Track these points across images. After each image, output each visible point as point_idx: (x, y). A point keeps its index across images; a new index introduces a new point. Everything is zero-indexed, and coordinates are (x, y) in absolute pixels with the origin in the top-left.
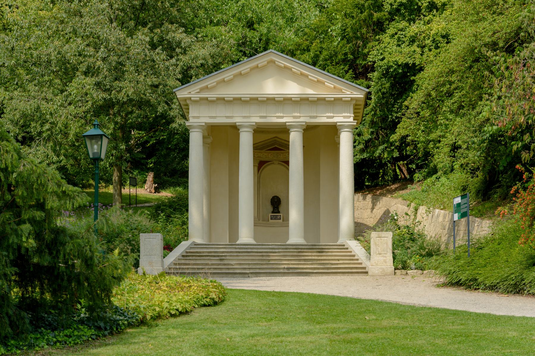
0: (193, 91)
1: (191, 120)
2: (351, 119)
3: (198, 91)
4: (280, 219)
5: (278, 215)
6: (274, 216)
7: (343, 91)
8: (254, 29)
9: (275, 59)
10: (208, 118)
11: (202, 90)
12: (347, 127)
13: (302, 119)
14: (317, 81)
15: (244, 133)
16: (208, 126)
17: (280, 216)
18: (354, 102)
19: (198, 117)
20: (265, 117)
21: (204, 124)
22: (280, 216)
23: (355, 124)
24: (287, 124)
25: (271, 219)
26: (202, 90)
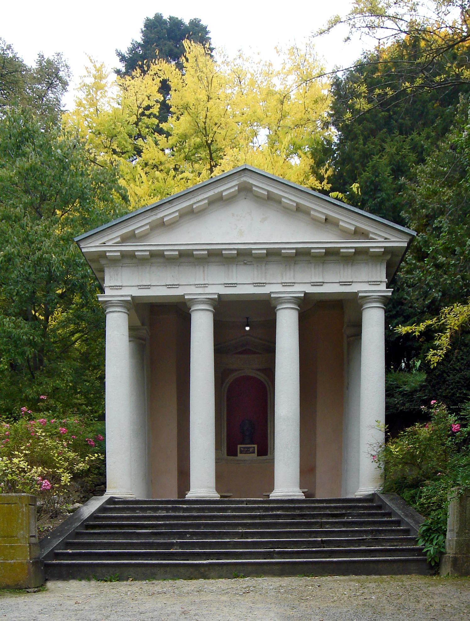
0: (108, 241)
1: (108, 292)
2: (383, 287)
3: (119, 239)
4: (254, 452)
5: (251, 447)
6: (244, 448)
7: (371, 235)
8: (134, 124)
9: (251, 181)
10: (165, 288)
11: (125, 239)
12: (289, 301)
13: (297, 288)
14: (326, 219)
15: (111, 314)
16: (138, 304)
17: (254, 447)
18: (389, 257)
19: (205, 285)
20: (148, 287)
21: (129, 298)
22: (254, 447)
23: (390, 294)
24: (272, 296)
25: (241, 452)
26: (125, 239)
